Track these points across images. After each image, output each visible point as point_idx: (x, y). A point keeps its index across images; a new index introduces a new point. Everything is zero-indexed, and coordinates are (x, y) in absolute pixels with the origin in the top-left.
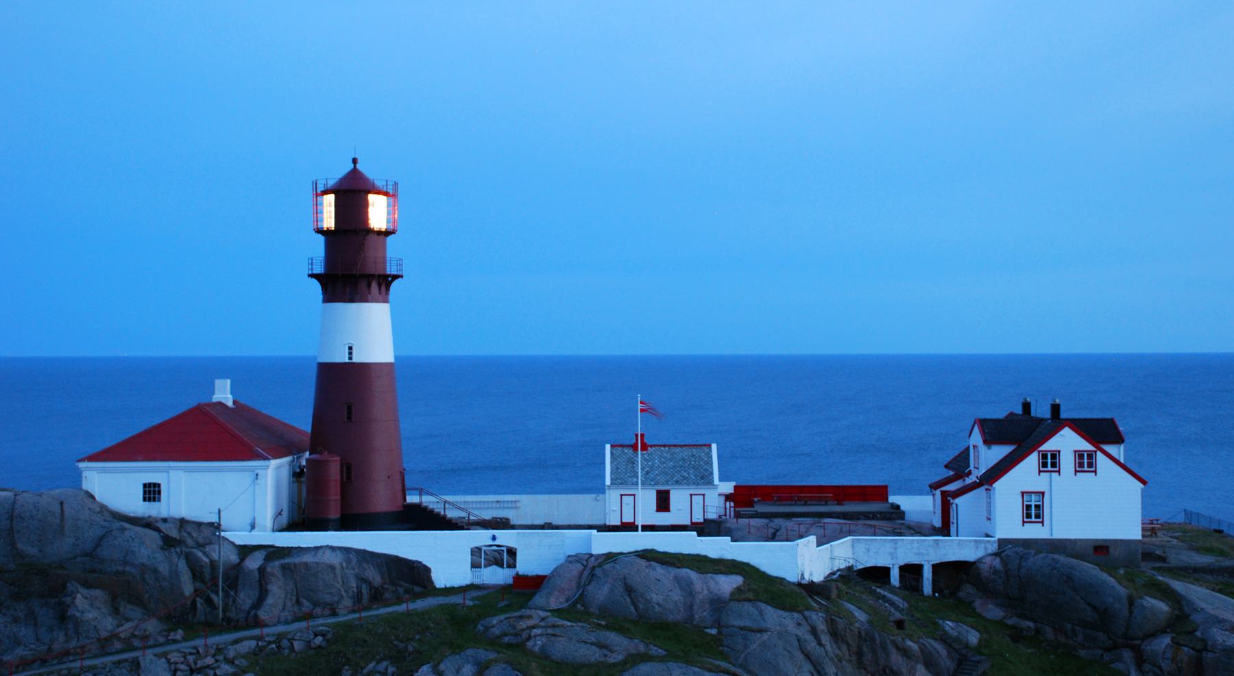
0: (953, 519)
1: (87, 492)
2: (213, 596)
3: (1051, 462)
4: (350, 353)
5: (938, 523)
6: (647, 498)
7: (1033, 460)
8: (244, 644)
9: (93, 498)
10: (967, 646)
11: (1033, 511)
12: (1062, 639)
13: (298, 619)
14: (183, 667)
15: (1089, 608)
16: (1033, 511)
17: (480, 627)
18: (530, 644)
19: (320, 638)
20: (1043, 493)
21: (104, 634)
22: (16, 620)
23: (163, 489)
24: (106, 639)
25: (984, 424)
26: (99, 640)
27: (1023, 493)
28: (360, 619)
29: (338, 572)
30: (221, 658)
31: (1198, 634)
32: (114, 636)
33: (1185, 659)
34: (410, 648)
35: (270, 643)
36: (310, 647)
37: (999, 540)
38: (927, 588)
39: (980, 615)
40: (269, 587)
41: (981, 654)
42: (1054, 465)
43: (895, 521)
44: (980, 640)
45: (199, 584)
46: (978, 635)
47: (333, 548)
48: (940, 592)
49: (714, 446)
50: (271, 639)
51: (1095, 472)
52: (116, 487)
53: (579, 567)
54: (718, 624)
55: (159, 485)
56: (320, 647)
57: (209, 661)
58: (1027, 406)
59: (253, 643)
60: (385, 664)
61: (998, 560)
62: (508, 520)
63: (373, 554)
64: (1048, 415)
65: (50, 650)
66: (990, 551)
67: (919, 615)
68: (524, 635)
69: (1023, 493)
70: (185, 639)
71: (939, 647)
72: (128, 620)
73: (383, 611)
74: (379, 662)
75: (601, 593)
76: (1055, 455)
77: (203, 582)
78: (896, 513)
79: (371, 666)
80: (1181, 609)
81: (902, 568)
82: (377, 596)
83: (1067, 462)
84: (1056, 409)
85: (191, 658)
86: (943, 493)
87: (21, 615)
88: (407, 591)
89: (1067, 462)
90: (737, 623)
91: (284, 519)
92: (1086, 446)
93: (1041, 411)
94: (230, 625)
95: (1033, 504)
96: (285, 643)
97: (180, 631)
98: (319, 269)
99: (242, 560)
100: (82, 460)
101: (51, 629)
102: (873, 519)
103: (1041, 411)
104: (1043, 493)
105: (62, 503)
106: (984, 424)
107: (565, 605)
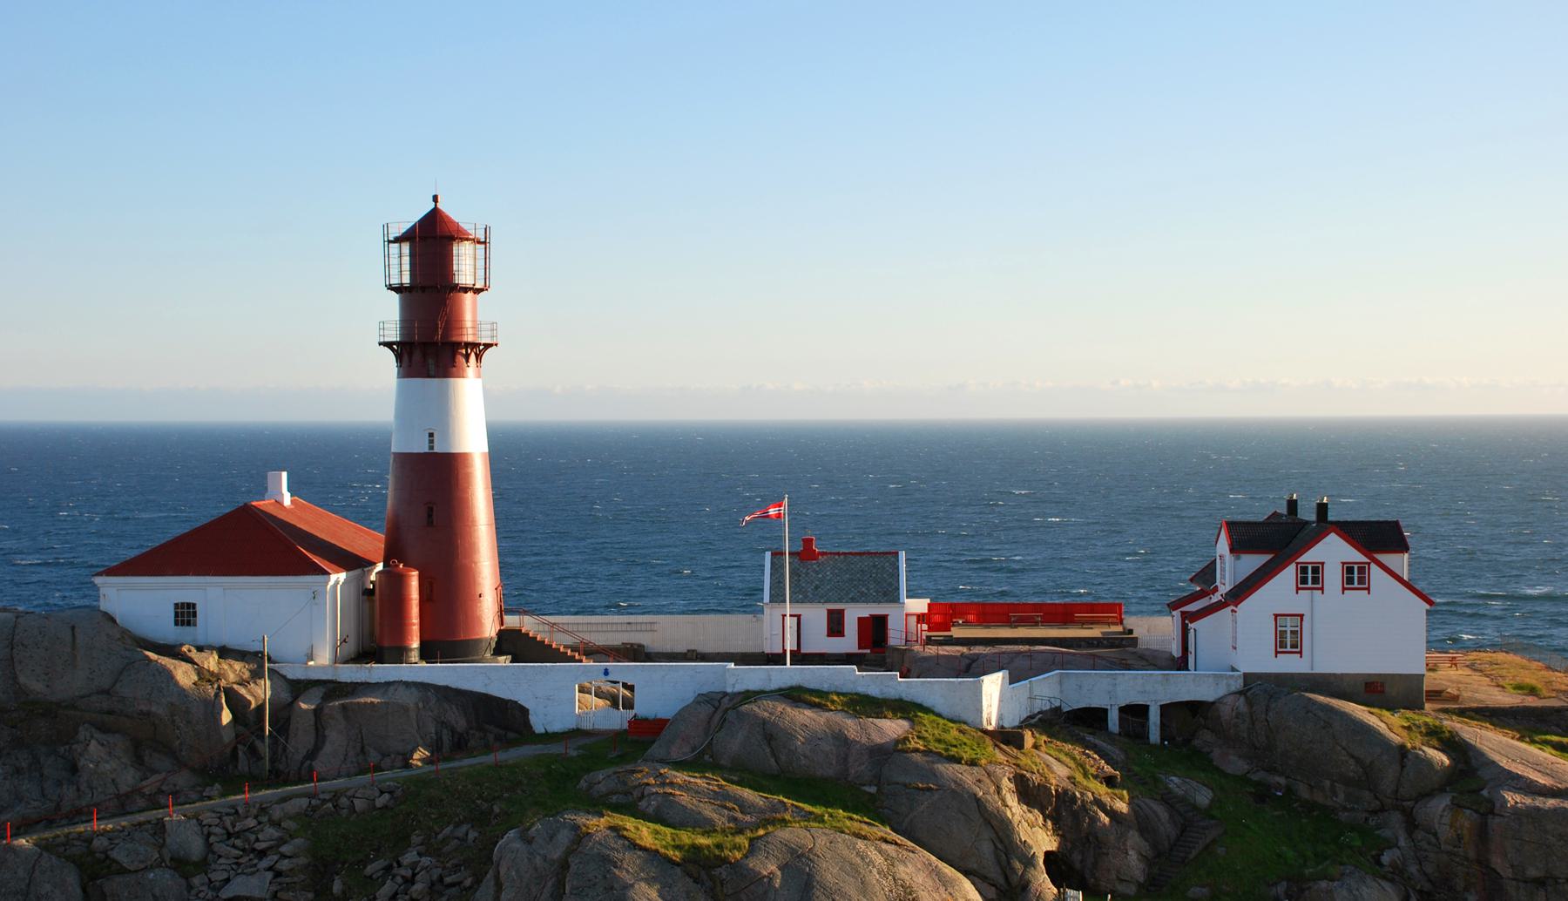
0: (1191, 648)
1: (106, 614)
2: (258, 743)
3: (1311, 577)
4: (431, 442)
5: (1176, 651)
6: (816, 616)
7: (1289, 574)
8: (290, 799)
9: (113, 620)
10: (1195, 807)
11: (1288, 639)
12: (1320, 799)
13: (362, 772)
14: (217, 830)
15: (1352, 762)
16: (1288, 639)
17: (583, 784)
18: (643, 804)
19: (387, 796)
20: (1302, 616)
21: (124, 789)
22: (18, 771)
23: (198, 609)
24: (127, 795)
25: (1231, 526)
26: (118, 796)
27: (1276, 616)
28: (437, 771)
29: (413, 714)
30: (265, 819)
31: (1485, 793)
32: (137, 791)
33: (1467, 824)
34: (496, 809)
35: (324, 801)
36: (374, 808)
37: (1246, 675)
38: (1154, 735)
39: (1217, 769)
40: (327, 733)
41: (1213, 817)
42: (1315, 580)
43: (1123, 652)
44: (1212, 801)
45: (241, 728)
46: (1210, 794)
47: (407, 684)
48: (1171, 739)
49: (903, 555)
50: (327, 797)
51: (1368, 589)
52: (143, 603)
53: (709, 709)
54: (878, 780)
55: (194, 605)
56: (386, 807)
57: (251, 822)
58: (1292, 505)
59: (304, 802)
60: (464, 828)
61: (1242, 699)
62: (641, 646)
63: (459, 693)
64: (1313, 518)
65: (58, 807)
66: (1233, 689)
67: (1136, 769)
68: (636, 794)
69: (1276, 616)
70: (223, 795)
71: (1161, 811)
72: (154, 771)
73: (467, 762)
74: (458, 825)
75: (734, 743)
76: (1317, 569)
77: (246, 725)
78: (1126, 641)
79: (448, 830)
80: (1467, 762)
81: (1123, 710)
82: (460, 745)
83: (1333, 577)
84: (1322, 509)
85: (228, 821)
86: (1183, 613)
87: (24, 765)
88: (498, 738)
89: (1333, 577)
90: (902, 779)
91: (351, 648)
92: (1356, 556)
93: (1307, 513)
94: (277, 777)
95: (1289, 629)
96: (344, 801)
97: (217, 786)
98: (394, 335)
99: (295, 698)
100: (99, 574)
101: (59, 784)
102: (1098, 647)
103: (1307, 513)
104: (1302, 616)
105: (73, 628)
106: (1231, 526)
107: (688, 757)
